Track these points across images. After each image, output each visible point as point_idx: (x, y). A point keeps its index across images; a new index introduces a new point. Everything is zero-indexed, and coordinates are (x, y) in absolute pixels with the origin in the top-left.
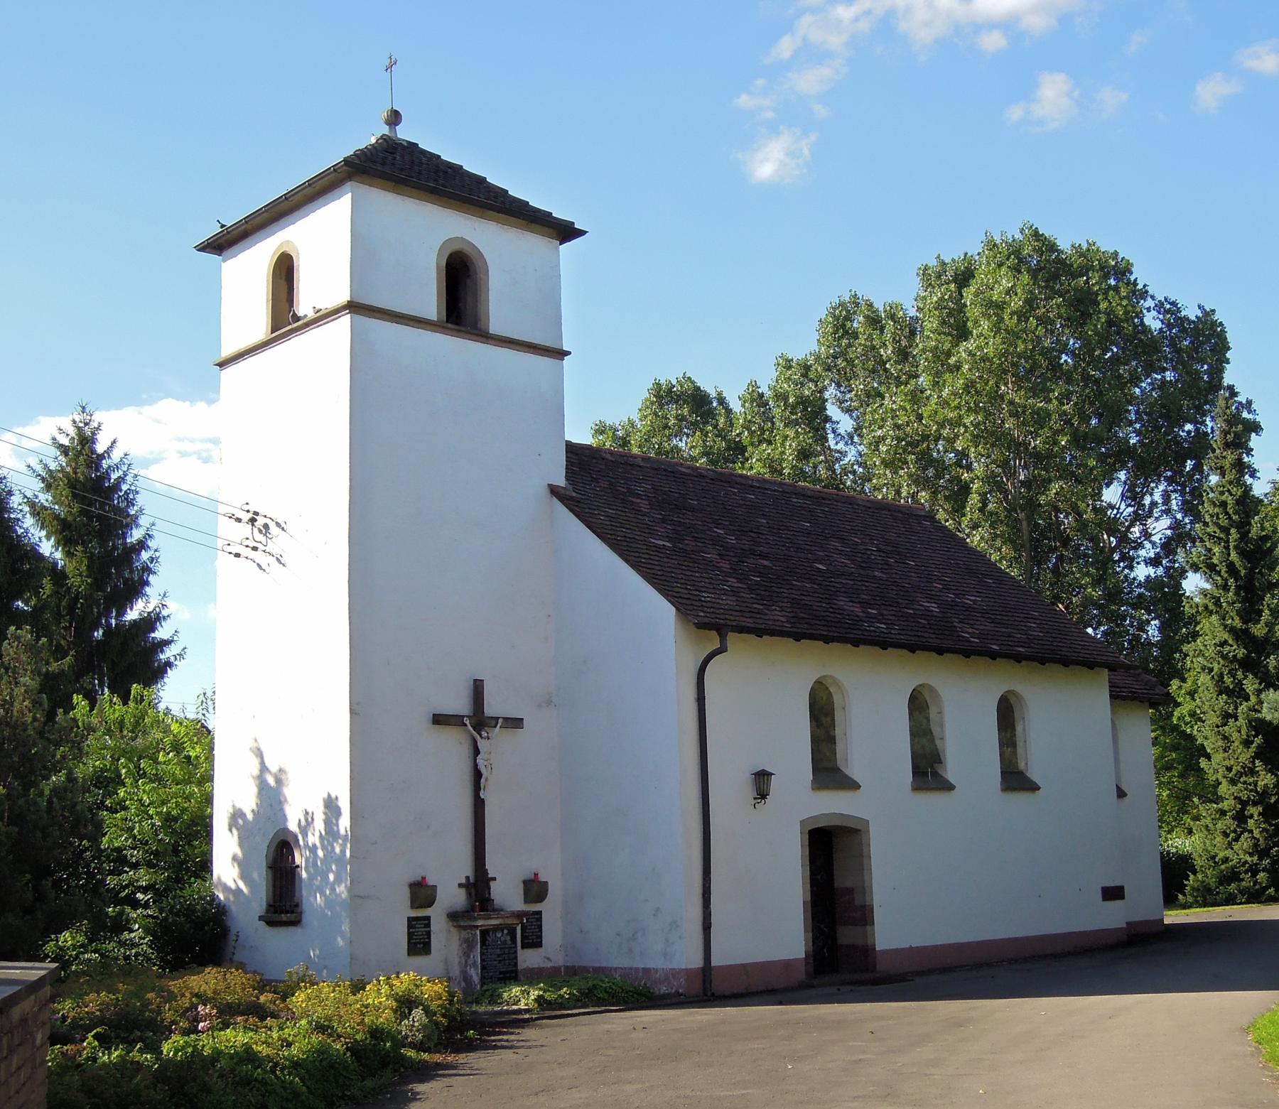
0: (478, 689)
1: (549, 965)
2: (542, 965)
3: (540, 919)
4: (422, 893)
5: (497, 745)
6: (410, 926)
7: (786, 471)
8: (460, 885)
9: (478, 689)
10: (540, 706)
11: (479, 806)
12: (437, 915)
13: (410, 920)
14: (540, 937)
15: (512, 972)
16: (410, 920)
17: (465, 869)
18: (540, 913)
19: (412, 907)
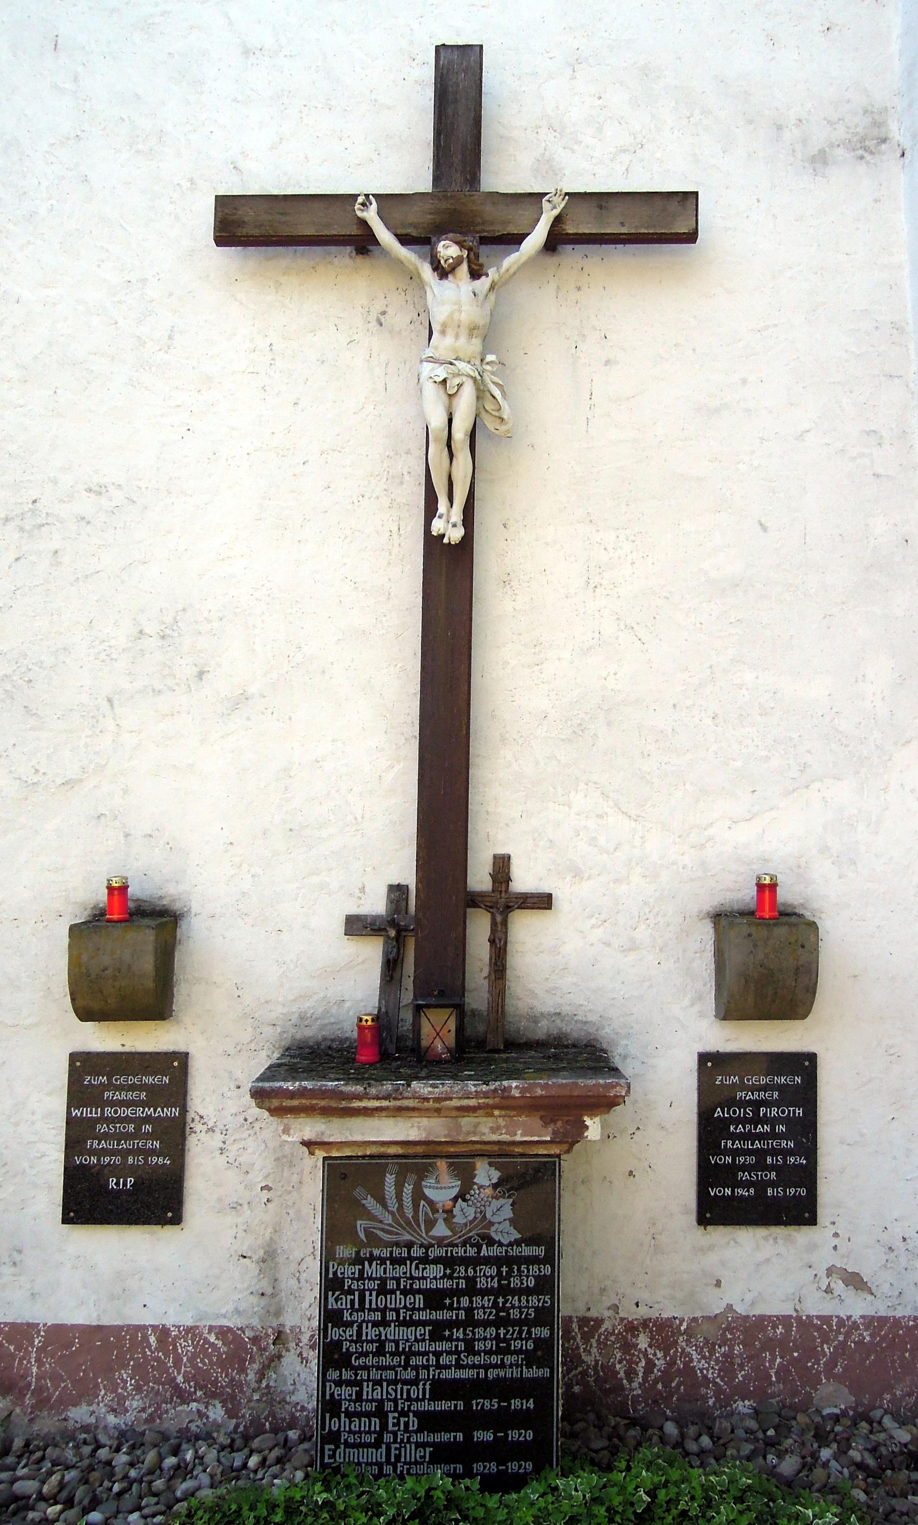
0: (458, 84)
1: (856, 1307)
2: (816, 1306)
3: (807, 1095)
4: (129, 952)
5: (600, 358)
6: (78, 1093)
7: (881, 1510)
8: (357, 926)
9: (458, 84)
10: (820, 160)
11: (449, 574)
12: (221, 1046)
13: (82, 1065)
14: (808, 1176)
15: (521, 1388)
16: (82, 1065)
17: (382, 857)
18: (804, 1066)
19: (731, 1009)
